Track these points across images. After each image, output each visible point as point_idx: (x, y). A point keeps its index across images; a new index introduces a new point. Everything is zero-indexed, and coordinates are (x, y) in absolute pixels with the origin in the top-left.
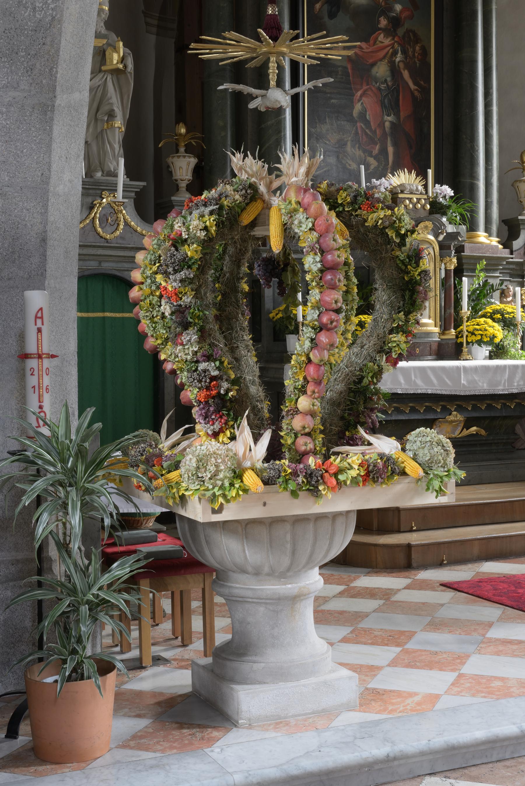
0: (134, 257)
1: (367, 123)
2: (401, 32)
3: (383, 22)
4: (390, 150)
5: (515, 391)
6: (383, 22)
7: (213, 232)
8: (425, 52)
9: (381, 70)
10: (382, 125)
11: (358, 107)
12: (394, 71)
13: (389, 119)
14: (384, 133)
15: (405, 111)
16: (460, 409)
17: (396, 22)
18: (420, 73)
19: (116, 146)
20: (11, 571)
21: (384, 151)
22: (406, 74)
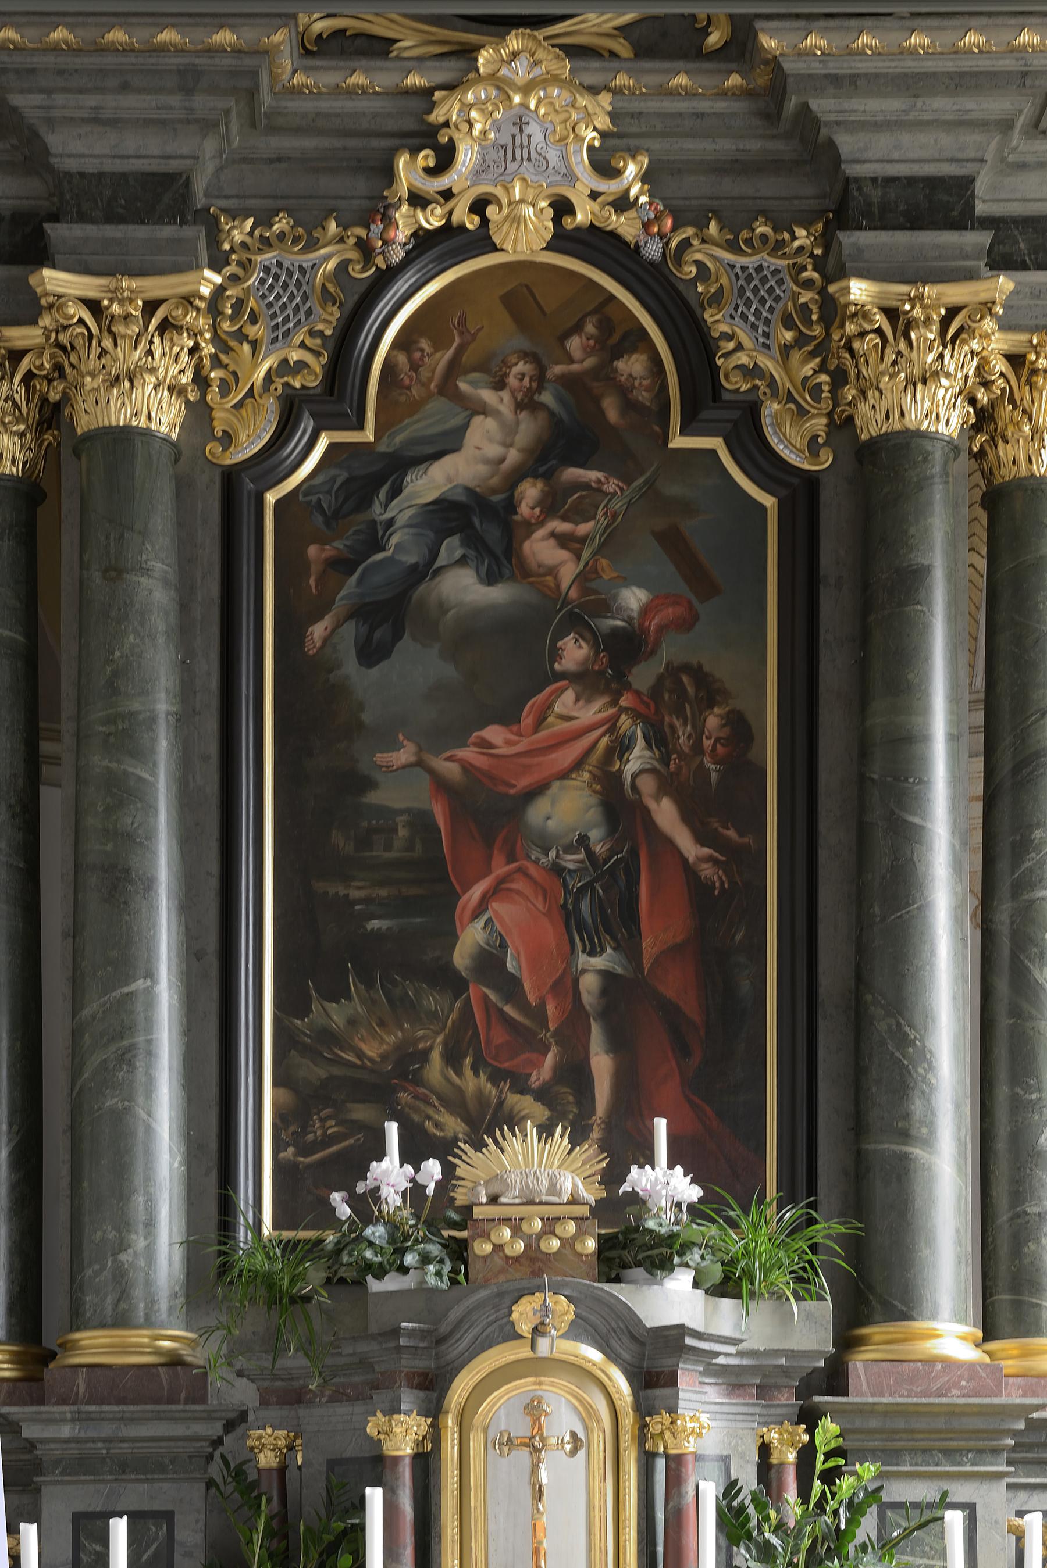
1: (511, 988)
2: (643, 676)
4: (602, 1065)
6: (574, 652)
8: (742, 731)
9: (567, 809)
10: (567, 985)
11: (472, 936)
12: (619, 806)
13: (593, 967)
14: (576, 1018)
15: (662, 928)
17: (623, 648)
18: (719, 802)
22: (666, 814)
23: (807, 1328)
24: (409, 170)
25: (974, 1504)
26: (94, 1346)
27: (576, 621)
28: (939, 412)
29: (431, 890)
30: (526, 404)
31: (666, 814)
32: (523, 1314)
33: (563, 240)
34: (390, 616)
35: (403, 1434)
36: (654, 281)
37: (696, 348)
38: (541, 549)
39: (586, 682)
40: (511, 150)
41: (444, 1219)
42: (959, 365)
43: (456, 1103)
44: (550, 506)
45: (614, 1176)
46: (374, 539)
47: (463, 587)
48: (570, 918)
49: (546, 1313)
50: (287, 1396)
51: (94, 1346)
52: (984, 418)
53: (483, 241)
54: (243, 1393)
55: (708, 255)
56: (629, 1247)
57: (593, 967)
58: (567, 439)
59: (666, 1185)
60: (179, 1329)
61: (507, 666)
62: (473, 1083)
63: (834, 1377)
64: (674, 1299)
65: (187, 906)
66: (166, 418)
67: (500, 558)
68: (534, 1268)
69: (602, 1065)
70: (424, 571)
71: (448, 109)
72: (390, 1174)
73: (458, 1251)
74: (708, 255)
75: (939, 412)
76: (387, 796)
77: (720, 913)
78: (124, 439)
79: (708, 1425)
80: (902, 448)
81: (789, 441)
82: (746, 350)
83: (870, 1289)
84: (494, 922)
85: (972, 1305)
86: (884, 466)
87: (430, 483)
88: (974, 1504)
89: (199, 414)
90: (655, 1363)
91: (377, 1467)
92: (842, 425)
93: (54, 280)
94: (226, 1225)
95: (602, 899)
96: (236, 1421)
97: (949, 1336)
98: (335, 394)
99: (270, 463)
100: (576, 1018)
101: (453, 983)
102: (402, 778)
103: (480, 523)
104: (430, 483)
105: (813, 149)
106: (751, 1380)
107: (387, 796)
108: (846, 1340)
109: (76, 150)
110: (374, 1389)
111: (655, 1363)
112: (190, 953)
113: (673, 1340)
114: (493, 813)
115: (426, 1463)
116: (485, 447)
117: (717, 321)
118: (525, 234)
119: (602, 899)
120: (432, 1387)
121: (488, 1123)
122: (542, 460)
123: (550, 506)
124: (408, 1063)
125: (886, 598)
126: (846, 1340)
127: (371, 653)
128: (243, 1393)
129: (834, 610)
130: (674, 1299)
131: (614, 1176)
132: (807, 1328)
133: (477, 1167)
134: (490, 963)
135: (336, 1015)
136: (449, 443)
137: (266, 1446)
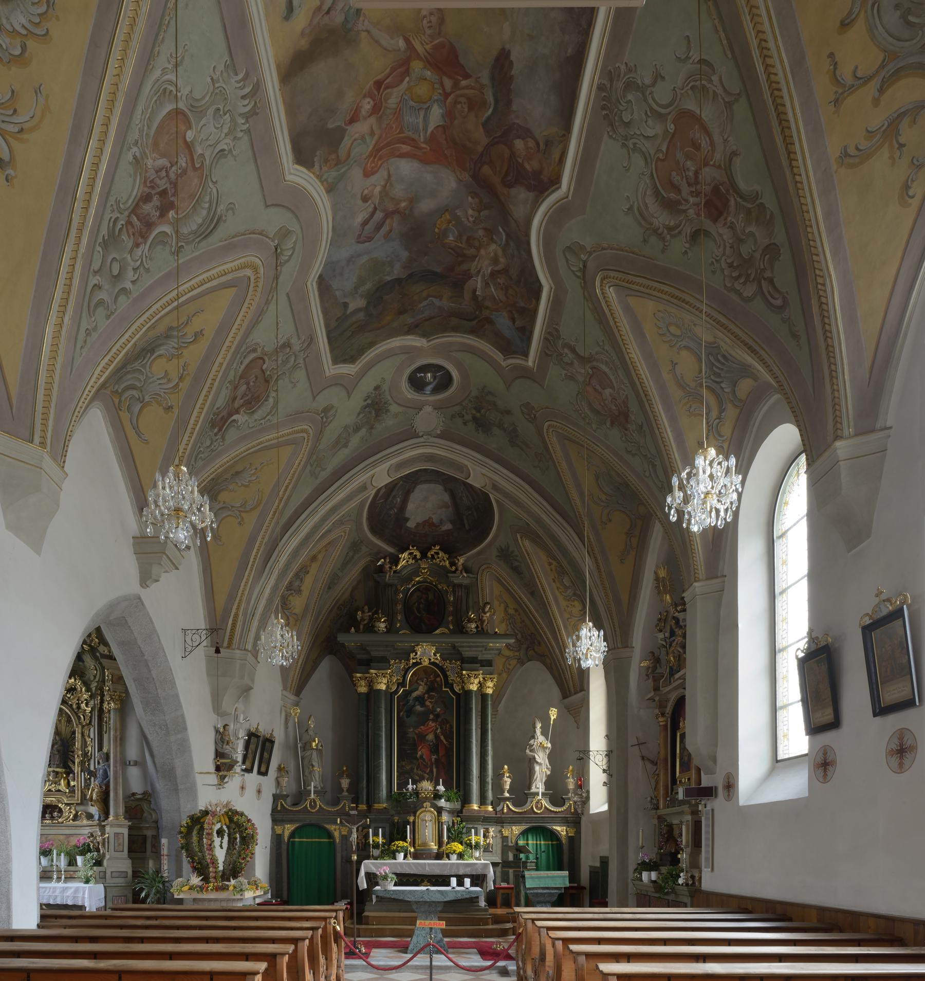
0: (38, 926)
1: (424, 760)
2: (440, 720)
3: (431, 717)
4: (435, 770)
5: (59, 903)
6: (431, 717)
7: (559, 828)
8: (451, 727)
9: (431, 737)
10: (431, 760)
11: (420, 753)
12: (437, 737)
13: (434, 757)
14: (432, 764)
15: (442, 752)
16: (575, 833)
17: (437, 716)
18: (449, 737)
19: (466, 463)
20: (428, 32)
21: (432, 771)
22: (442, 738)
23: (457, 805)
24: (412, 655)
25: (875, 715)
26: (376, 806)
27: (432, 713)
28: (474, 687)
29: (415, 747)
30: (426, 684)
31: (442, 738)
32: (425, 805)
33: (430, 663)
34: (410, 712)
35: (411, 819)
36: (441, 669)
37: (446, 677)
38: (428, 703)
39: (433, 720)
40: (423, 654)
41: (416, 793)
42: (476, 681)
43: (418, 775)
44: (429, 698)
45: (435, 787)
46: (408, 702)
47: (418, 708)
48: (431, 751)
49: (427, 804)
50: (399, 813)
51: (376, 806)
52: (481, 686)
53: (421, 663)
54: (393, 812)
55: (447, 664)
56: (437, 796)
57: (434, 757)
58: (431, 689)
59: (441, 788)
60: (291, 110)
61: (423, 718)
62: (420, 772)
63: (461, 811)
64: (442, 803)
65: (386, 720)
66: (383, 687)
67: (423, 704)
68: (426, 799)
69: (435, 770)
70: (414, 706)
71: (416, 648)
72: (410, 787)
73: (418, 796)
74: (447, 664)
75: (474, 687)
76: (410, 735)
77: (449, 750)
78: (380, 690)
79: (445, 817)
80: (470, 691)
81: (457, 689)
82: (452, 677)
83: (466, 800)
84: (422, 752)
85: (479, 801)
86: (469, 693)
87: (415, 694)
88: (875, 715)
89: (388, 687)
90: (440, 810)
91: (409, 823)
92: (463, 687)
93: (372, 671)
94: (391, 791)
95: (435, 749)
96: (392, 816)
97: (475, 807)
98: (402, 684)
99: (396, 691)
100: (432, 764)
101: (417, 759)
102: (411, 732)
103: (420, 700)
104: (415, 694)
105: (459, 653)
106: (451, 812)
107: (410, 735)
108: (463, 807)
109: (374, 654)
110: (409, 813)
111: (440, 810)
112: (387, 755)
113: (441, 808)
114: (422, 737)
115: (414, 822)
116: (421, 690)
117: (448, 673)
118: (426, 663)
119: (435, 749)
120: (415, 813)
121: (422, 779)
122: (428, 691)
123: (429, 698)
124: (412, 769)
125: (468, 711)
126: (463, 807)
127: (408, 716)
128: (393, 812)
129: (462, 710)
130: (442, 803)
131: (435, 787)
132: (457, 805)
133: (420, 785)
134: (421, 757)
135: (404, 763)
136: (417, 689)
137: (396, 819)
